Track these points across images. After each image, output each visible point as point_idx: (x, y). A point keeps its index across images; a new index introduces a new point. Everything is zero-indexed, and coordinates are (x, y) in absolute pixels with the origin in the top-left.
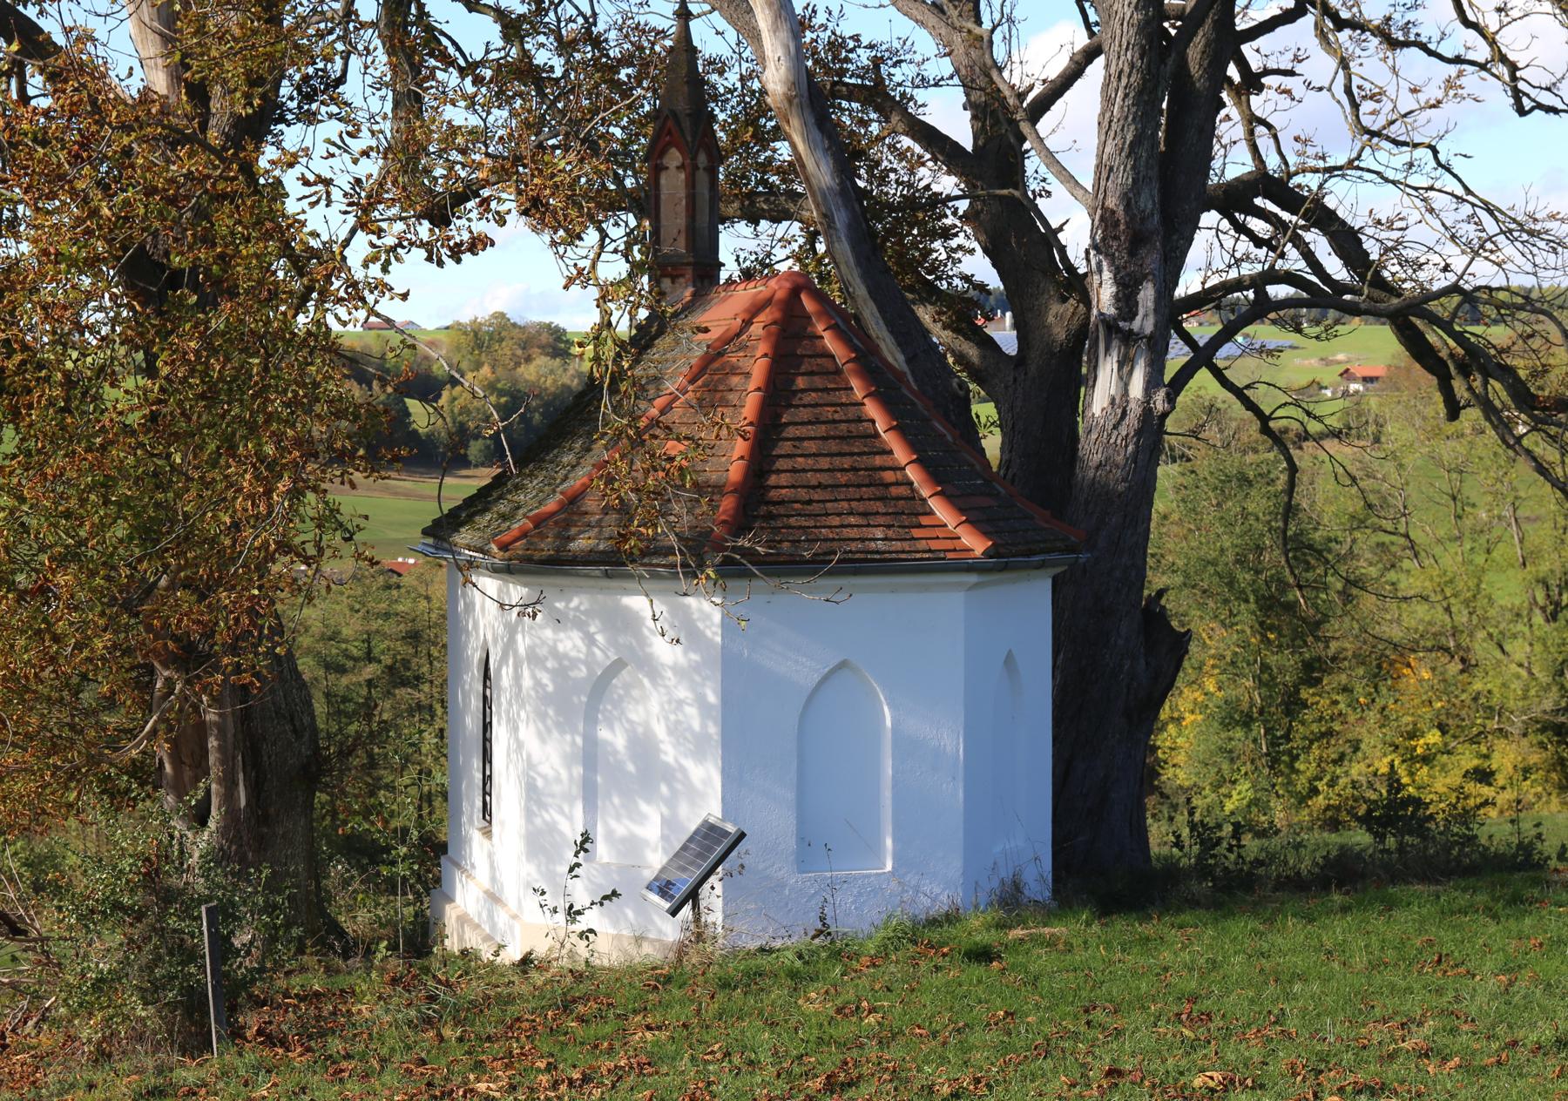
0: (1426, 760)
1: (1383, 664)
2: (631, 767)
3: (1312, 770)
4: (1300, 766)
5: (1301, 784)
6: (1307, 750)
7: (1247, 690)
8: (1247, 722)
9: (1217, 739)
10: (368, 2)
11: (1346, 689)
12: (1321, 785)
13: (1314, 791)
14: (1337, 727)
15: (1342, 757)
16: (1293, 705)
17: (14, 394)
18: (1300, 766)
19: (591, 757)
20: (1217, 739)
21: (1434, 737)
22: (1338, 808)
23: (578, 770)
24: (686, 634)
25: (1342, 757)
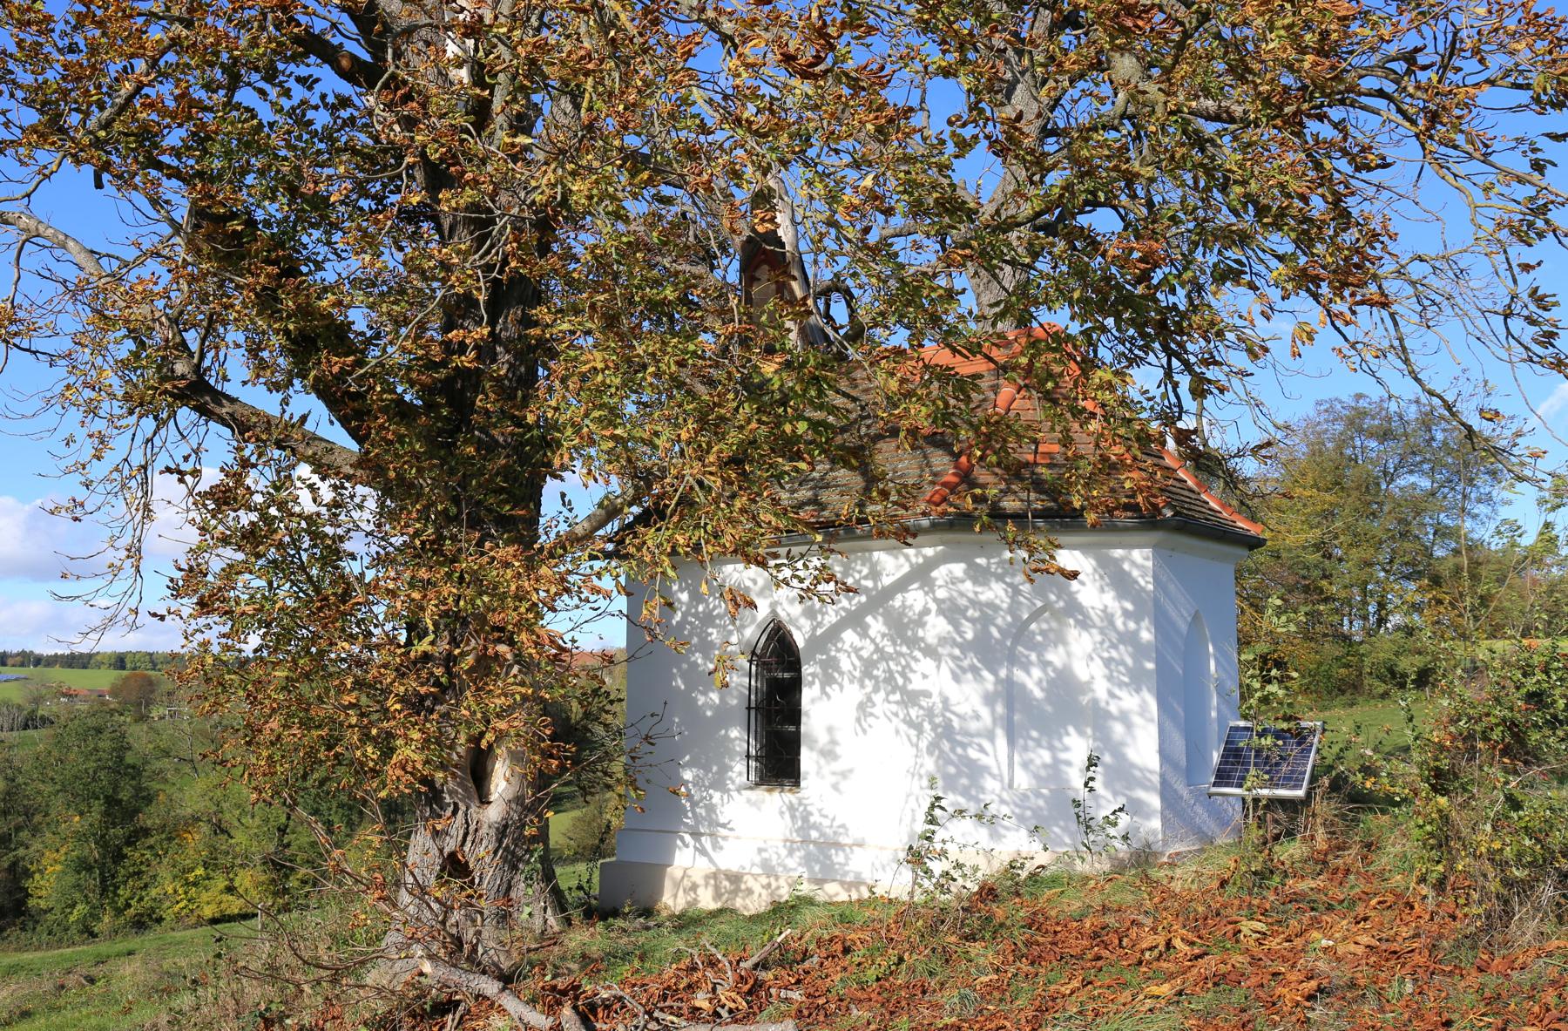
0: (195, 884)
1: (173, 832)
2: (1049, 709)
3: (128, 894)
4: (120, 892)
5: (121, 903)
6: (125, 883)
7: (93, 851)
8: (89, 869)
9: (71, 879)
10: (840, 2)
11: (151, 847)
12: (133, 902)
13: (128, 906)
14: (143, 868)
15: (146, 886)
16: (119, 857)
17: (823, 97)
18: (120, 892)
19: (1010, 694)
20: (71, 879)
21: (200, 871)
22: (142, 915)
23: (1000, 709)
24: (1120, 582)
25: (146, 886)
